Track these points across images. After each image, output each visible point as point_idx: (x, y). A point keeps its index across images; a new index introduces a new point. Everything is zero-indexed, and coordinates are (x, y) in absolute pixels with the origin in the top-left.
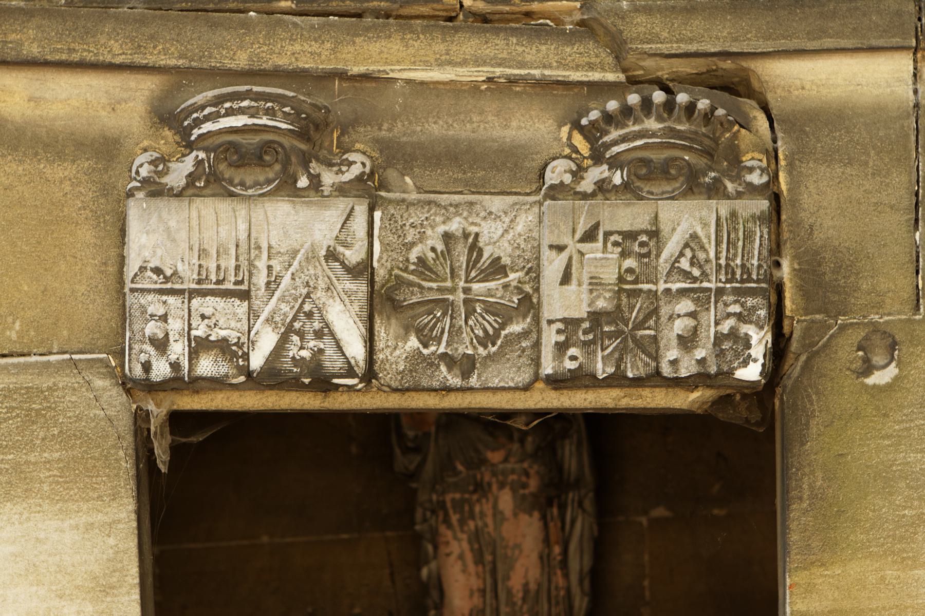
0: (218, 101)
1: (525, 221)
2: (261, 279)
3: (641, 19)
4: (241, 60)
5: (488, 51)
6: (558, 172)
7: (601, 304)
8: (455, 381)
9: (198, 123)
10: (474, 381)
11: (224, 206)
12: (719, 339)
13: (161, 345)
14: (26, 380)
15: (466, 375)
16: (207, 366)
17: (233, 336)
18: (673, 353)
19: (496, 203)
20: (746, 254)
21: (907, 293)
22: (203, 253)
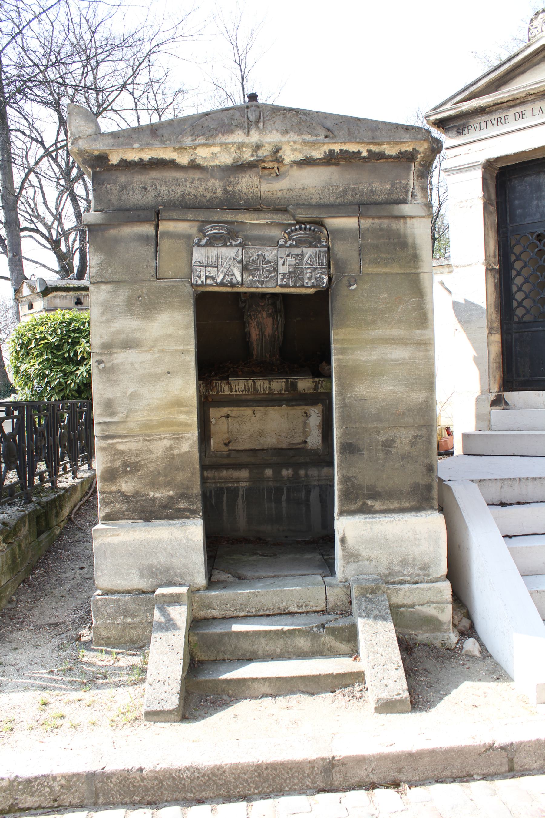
0: (212, 227)
1: (274, 252)
4: (216, 219)
6: (281, 242)
7: (291, 270)
8: (259, 286)
9: (207, 232)
10: (264, 286)
12: (317, 278)
13: (200, 277)
14: (173, 284)
15: (262, 285)
16: (209, 282)
17: (214, 275)
18: (306, 281)
19: (269, 248)
21: (358, 269)
22: (208, 258)
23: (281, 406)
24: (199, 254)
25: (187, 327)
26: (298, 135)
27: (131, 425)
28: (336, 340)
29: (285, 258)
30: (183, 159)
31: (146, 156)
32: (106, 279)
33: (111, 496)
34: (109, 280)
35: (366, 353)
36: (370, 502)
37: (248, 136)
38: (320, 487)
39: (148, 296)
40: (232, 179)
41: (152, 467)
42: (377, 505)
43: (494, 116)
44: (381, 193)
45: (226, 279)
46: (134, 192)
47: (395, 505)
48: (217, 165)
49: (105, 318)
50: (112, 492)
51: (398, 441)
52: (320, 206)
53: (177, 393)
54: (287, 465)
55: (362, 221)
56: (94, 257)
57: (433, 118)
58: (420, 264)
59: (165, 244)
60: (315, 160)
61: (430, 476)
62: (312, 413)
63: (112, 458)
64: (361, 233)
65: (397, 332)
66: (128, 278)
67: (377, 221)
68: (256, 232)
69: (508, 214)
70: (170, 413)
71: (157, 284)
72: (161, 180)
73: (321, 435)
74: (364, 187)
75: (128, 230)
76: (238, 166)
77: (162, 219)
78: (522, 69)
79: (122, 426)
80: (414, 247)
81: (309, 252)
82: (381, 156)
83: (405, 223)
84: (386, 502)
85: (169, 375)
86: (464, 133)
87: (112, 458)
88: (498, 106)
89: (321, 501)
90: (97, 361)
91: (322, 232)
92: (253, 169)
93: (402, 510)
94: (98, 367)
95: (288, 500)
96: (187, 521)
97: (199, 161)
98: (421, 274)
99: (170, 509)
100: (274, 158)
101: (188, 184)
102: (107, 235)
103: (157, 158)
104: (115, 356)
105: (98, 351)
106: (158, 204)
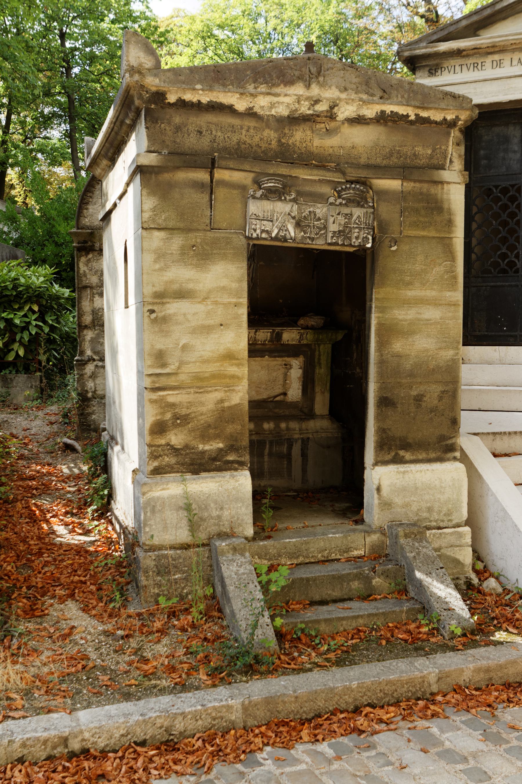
0: (268, 180)
1: (325, 209)
2: (275, 218)
3: (349, 169)
4: (271, 171)
5: (319, 173)
6: (332, 200)
7: (341, 229)
8: (310, 242)
9: (263, 184)
10: (314, 243)
11: (268, 202)
12: (363, 238)
13: (255, 230)
14: (227, 235)
15: (312, 241)
16: (264, 235)
17: (269, 229)
18: (354, 240)
19: (319, 205)
20: (369, 220)
21: (399, 231)
22: (264, 212)
23: (264, 357)
24: (254, 207)
25: (240, 281)
26: (356, 93)
27: (182, 377)
28: (377, 299)
29: (335, 216)
30: (241, 105)
31: (205, 100)
32: (159, 224)
33: (160, 449)
34: (162, 227)
35: (403, 312)
36: (402, 453)
37: (308, 89)
38: (303, 439)
39: (202, 246)
40: (287, 131)
41: (203, 419)
42: (408, 456)
43: (471, 61)
44: (423, 157)
45: (281, 234)
46: (189, 135)
47: (422, 455)
48: (272, 115)
49: (157, 266)
50: (161, 445)
51: (428, 396)
52: (368, 166)
53: (229, 345)
54: (268, 418)
55: (405, 184)
56: (147, 201)
57: (406, 54)
58: (453, 229)
59: (220, 193)
60: (365, 120)
61: (454, 429)
62: (294, 364)
63: (162, 410)
64: (403, 196)
65: (430, 293)
66: (182, 225)
67: (418, 185)
68: (308, 188)
69: (472, 165)
70: (222, 365)
71: (210, 235)
72: (217, 125)
73: (301, 387)
74: (407, 150)
75: (182, 175)
76: (294, 118)
77: (218, 167)
78: (503, 15)
79: (173, 378)
80: (450, 212)
81: (357, 212)
82: (427, 121)
83: (443, 189)
84: (416, 452)
85: (222, 327)
86: (437, 74)
87: (162, 410)
88: (476, 51)
89: (303, 455)
90: (149, 311)
91: (368, 192)
92: (307, 123)
93: (429, 461)
94: (149, 317)
95: (270, 454)
96: (235, 473)
97: (257, 109)
98: (454, 239)
99: (219, 461)
100: (329, 114)
101: (244, 132)
102: (160, 178)
103: (216, 102)
104: (168, 306)
105: (150, 300)
106: (213, 150)
